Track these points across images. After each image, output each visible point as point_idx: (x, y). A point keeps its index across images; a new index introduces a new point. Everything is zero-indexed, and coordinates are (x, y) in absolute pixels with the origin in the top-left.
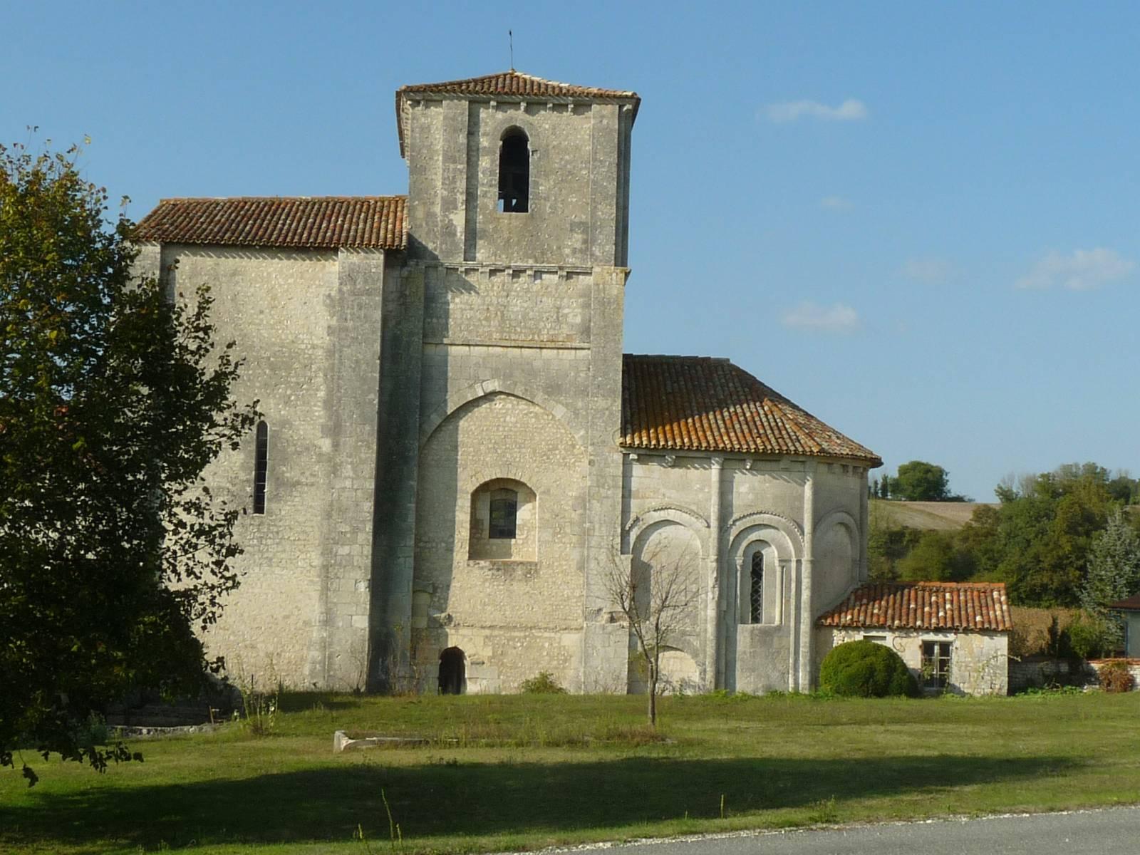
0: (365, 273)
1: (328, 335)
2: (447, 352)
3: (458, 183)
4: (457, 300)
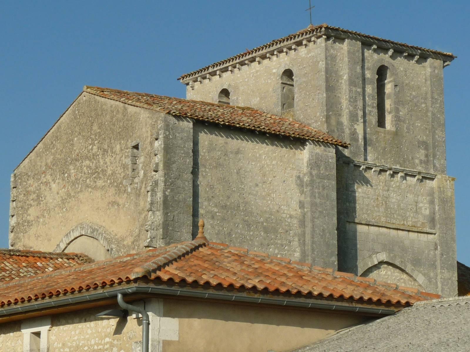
0: (326, 162)
1: (300, 208)
2: (356, 229)
3: (358, 102)
4: (360, 190)
